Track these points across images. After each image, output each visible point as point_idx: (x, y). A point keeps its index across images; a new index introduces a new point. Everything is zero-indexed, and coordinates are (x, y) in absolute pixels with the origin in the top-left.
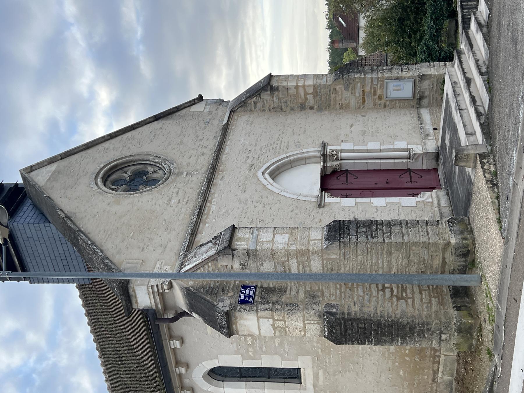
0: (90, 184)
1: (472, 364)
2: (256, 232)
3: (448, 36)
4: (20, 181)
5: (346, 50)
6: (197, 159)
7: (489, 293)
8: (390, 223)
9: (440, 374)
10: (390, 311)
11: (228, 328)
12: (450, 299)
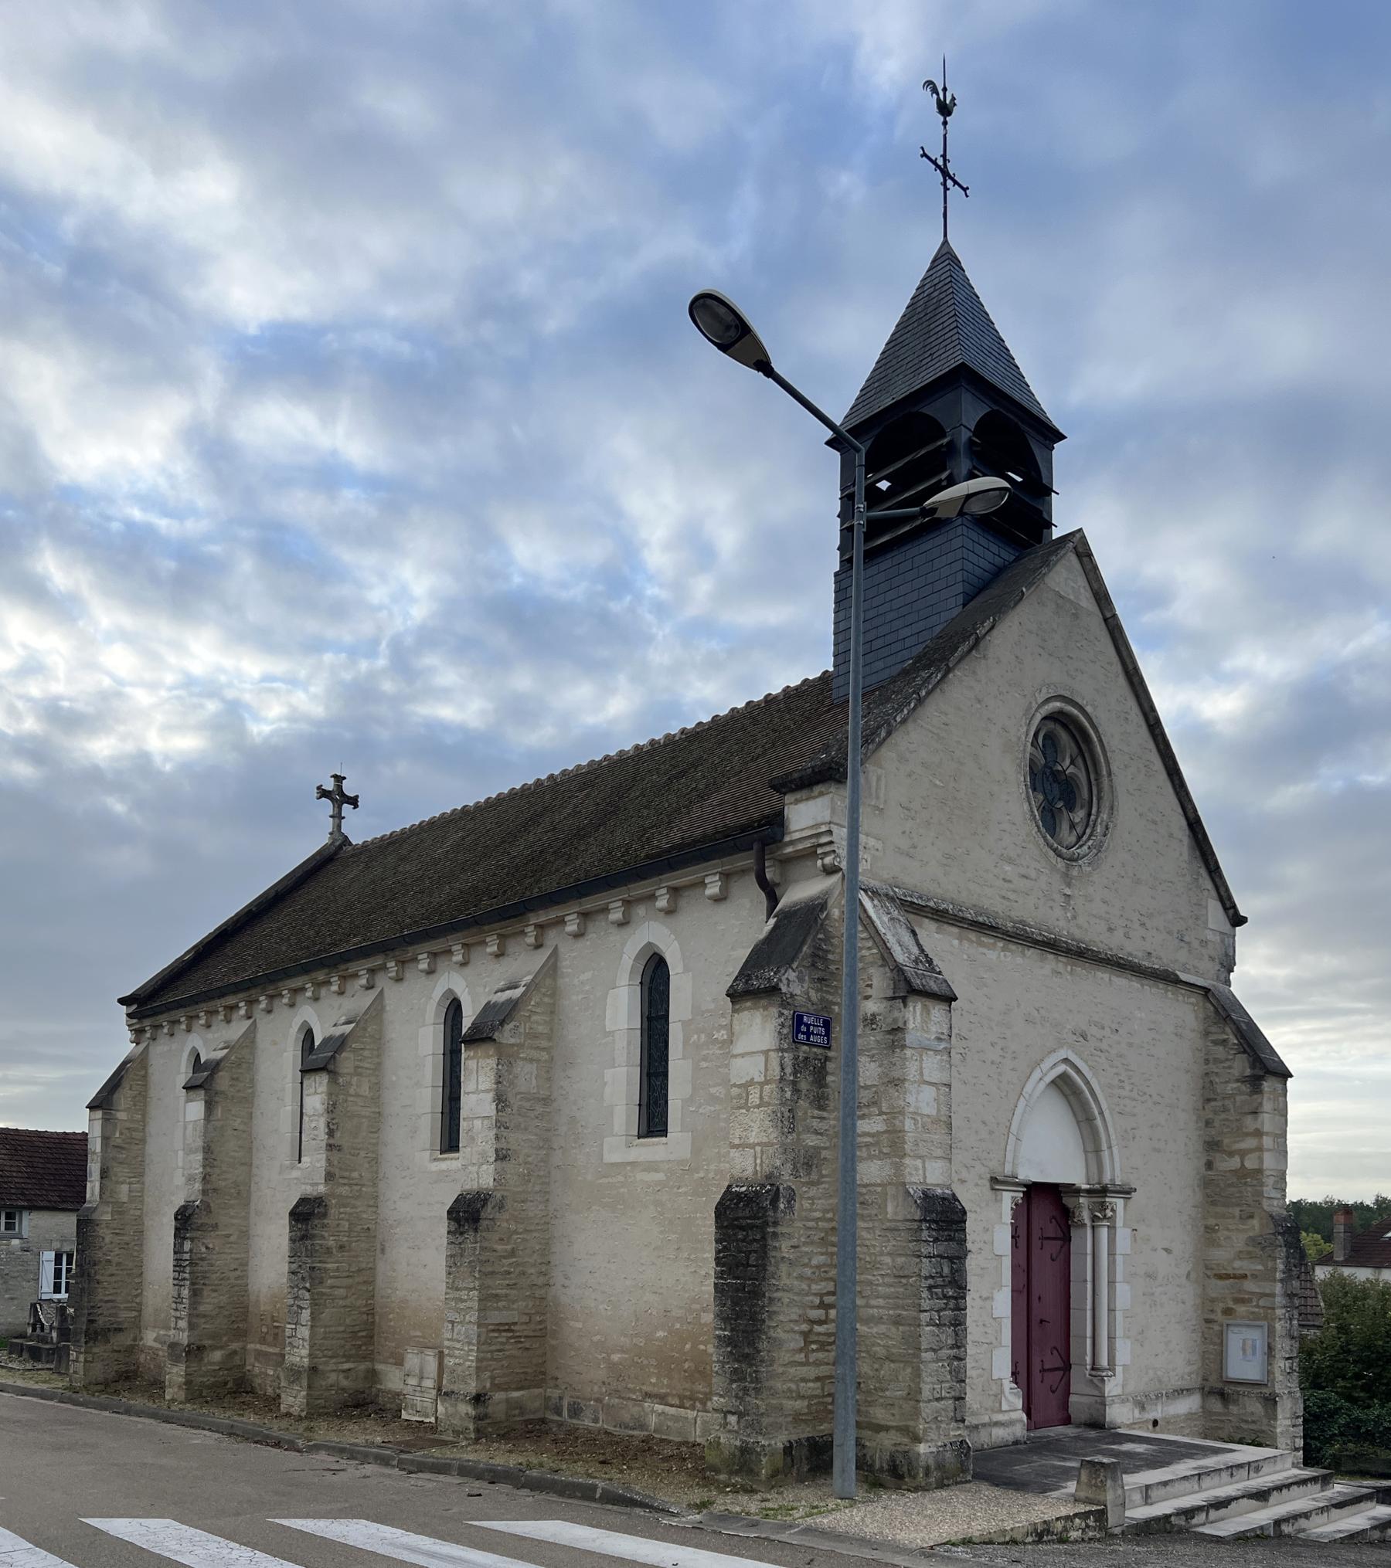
0: (1049, 686)
1: (680, 1470)
2: (942, 1045)
3: (1355, 1458)
4: (1056, 533)
5: (1328, 1239)
6: (1100, 918)
7: (820, 1513)
8: (960, 1325)
9: (659, 1408)
10: (781, 1318)
11: (749, 989)
12: (806, 1435)
